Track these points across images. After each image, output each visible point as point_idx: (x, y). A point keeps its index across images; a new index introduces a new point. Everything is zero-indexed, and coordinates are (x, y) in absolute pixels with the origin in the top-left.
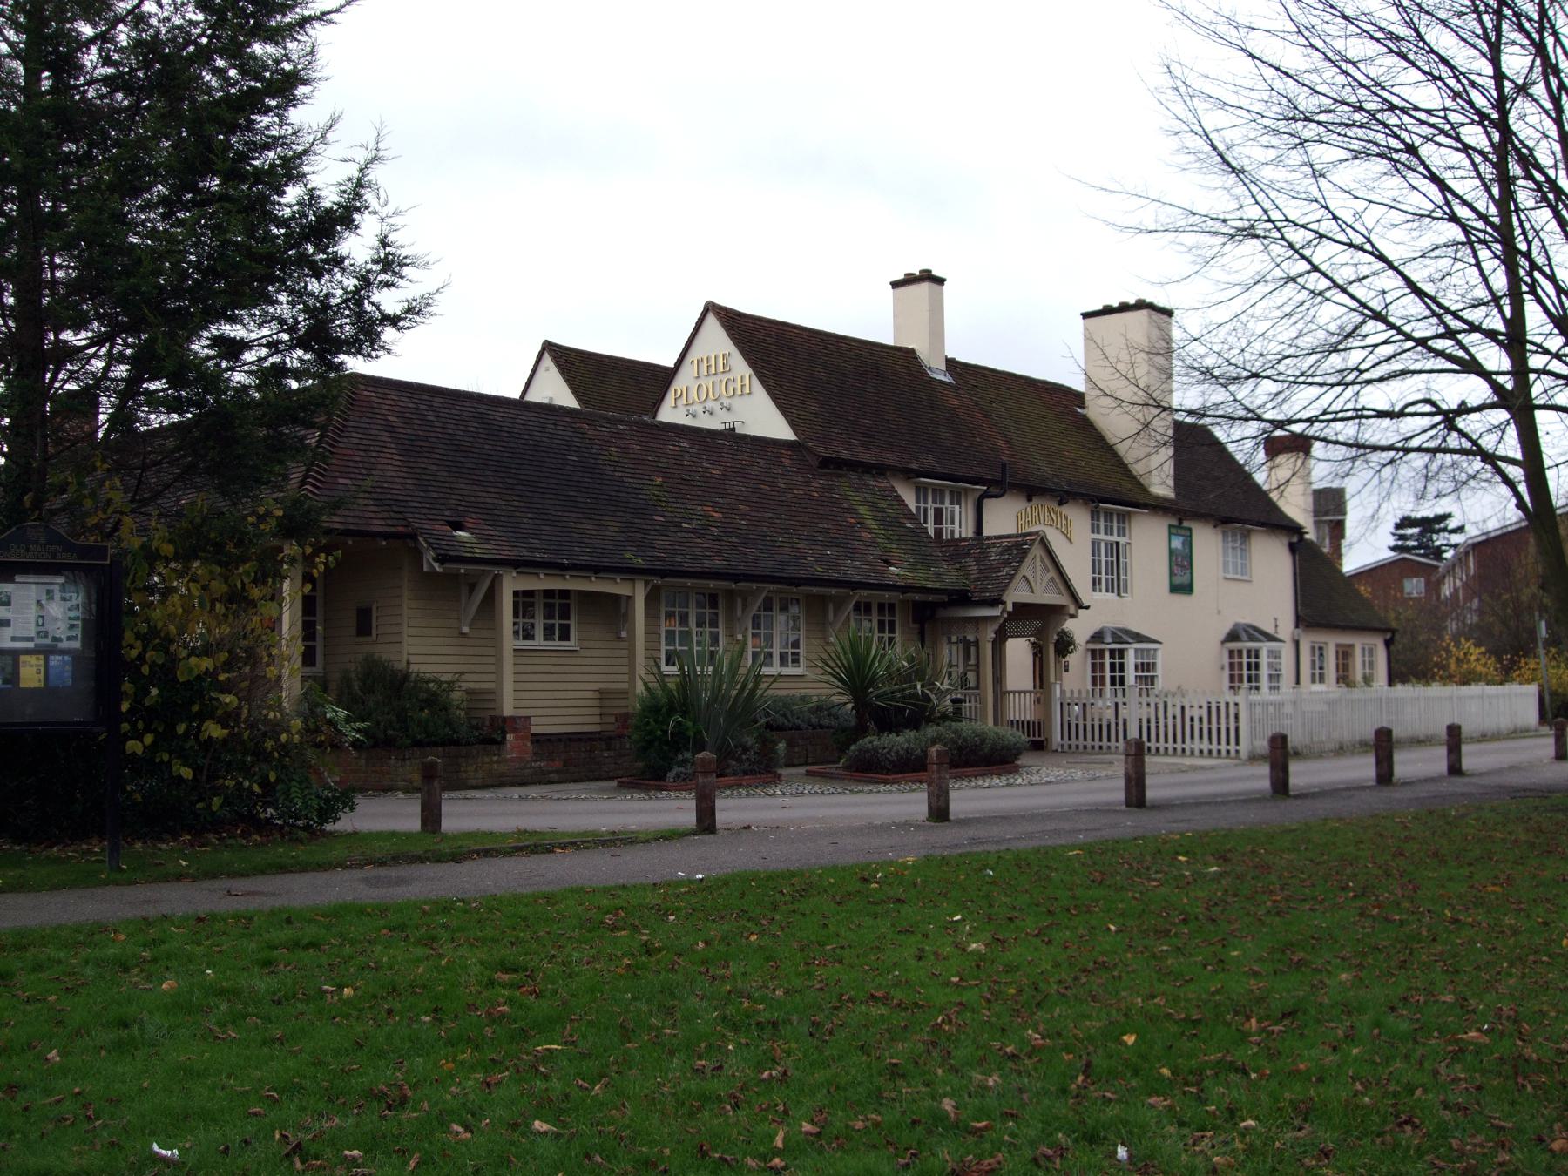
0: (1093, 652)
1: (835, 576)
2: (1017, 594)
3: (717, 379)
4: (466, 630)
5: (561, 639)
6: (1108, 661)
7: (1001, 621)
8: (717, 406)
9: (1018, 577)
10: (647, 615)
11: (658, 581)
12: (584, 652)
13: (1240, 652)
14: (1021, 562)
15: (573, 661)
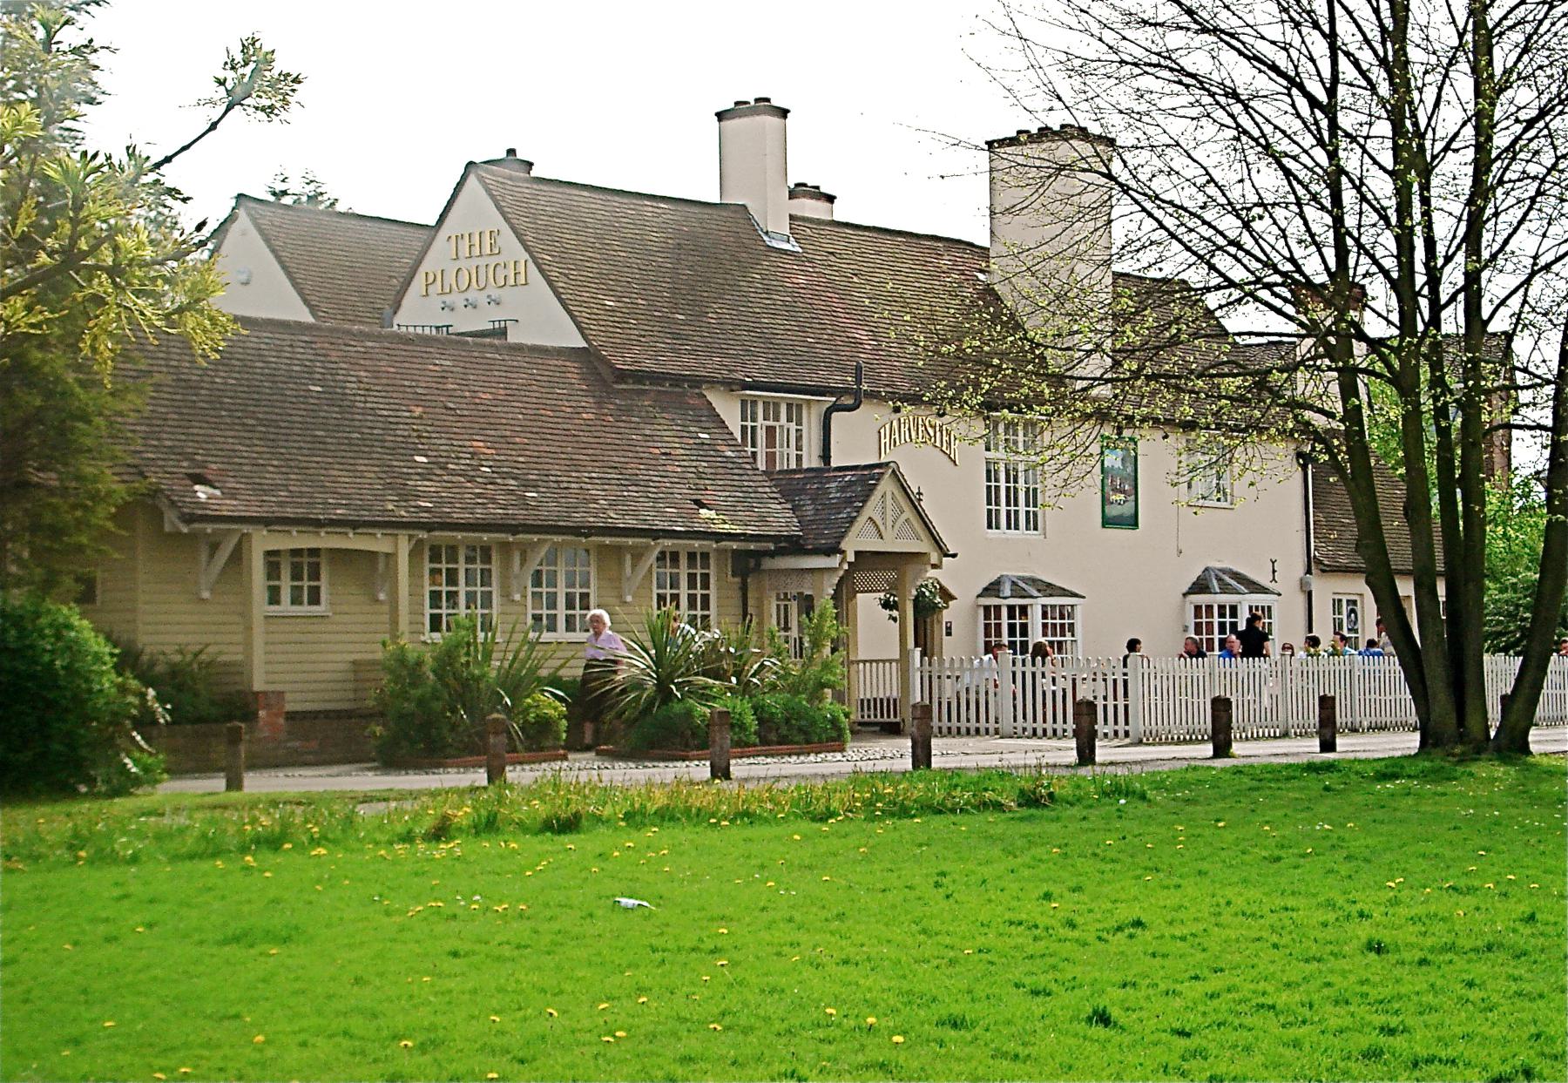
0: (987, 609)
1: (631, 522)
2: (857, 541)
3: (482, 262)
4: (206, 595)
5: (310, 603)
6: (1005, 621)
7: (841, 573)
8: (481, 298)
9: (862, 519)
10: (411, 574)
11: (423, 535)
12: (337, 618)
13: (1209, 608)
14: (864, 502)
15: (322, 628)
